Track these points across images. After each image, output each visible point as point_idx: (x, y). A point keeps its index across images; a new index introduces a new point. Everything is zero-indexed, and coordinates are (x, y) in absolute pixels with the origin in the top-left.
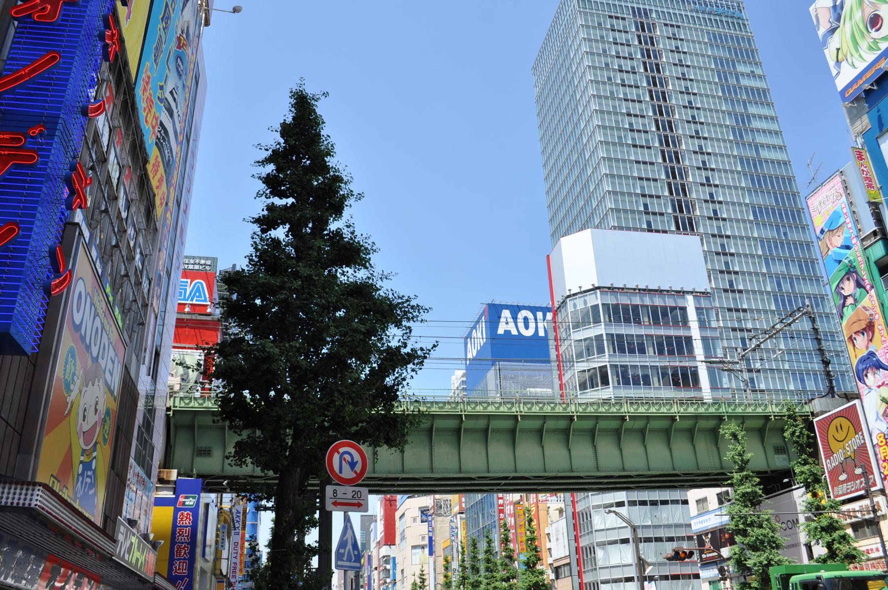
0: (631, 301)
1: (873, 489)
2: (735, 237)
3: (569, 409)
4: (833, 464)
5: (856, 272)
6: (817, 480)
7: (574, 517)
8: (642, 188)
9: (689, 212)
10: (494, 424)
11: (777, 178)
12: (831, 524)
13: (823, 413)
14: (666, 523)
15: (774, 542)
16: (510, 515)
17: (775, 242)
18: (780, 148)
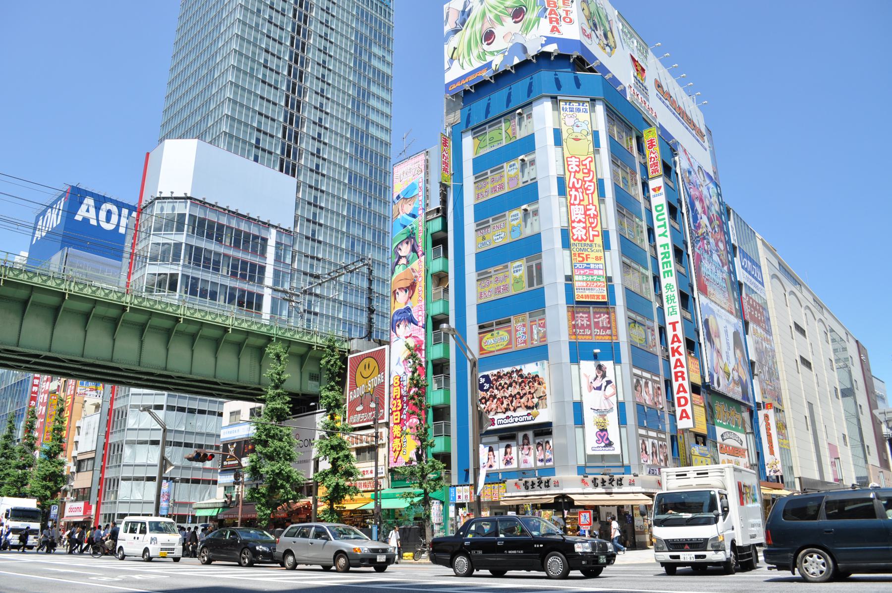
0: (218, 219)
1: (380, 421)
2: (328, 194)
3: (123, 299)
4: (355, 397)
5: (414, 238)
6: (338, 406)
7: (109, 413)
8: (259, 123)
9: (295, 158)
10: (36, 297)
11: (376, 154)
12: (339, 444)
13: (357, 351)
14: (198, 431)
15: (289, 455)
16: (42, 404)
17: (360, 208)
18: (387, 130)
